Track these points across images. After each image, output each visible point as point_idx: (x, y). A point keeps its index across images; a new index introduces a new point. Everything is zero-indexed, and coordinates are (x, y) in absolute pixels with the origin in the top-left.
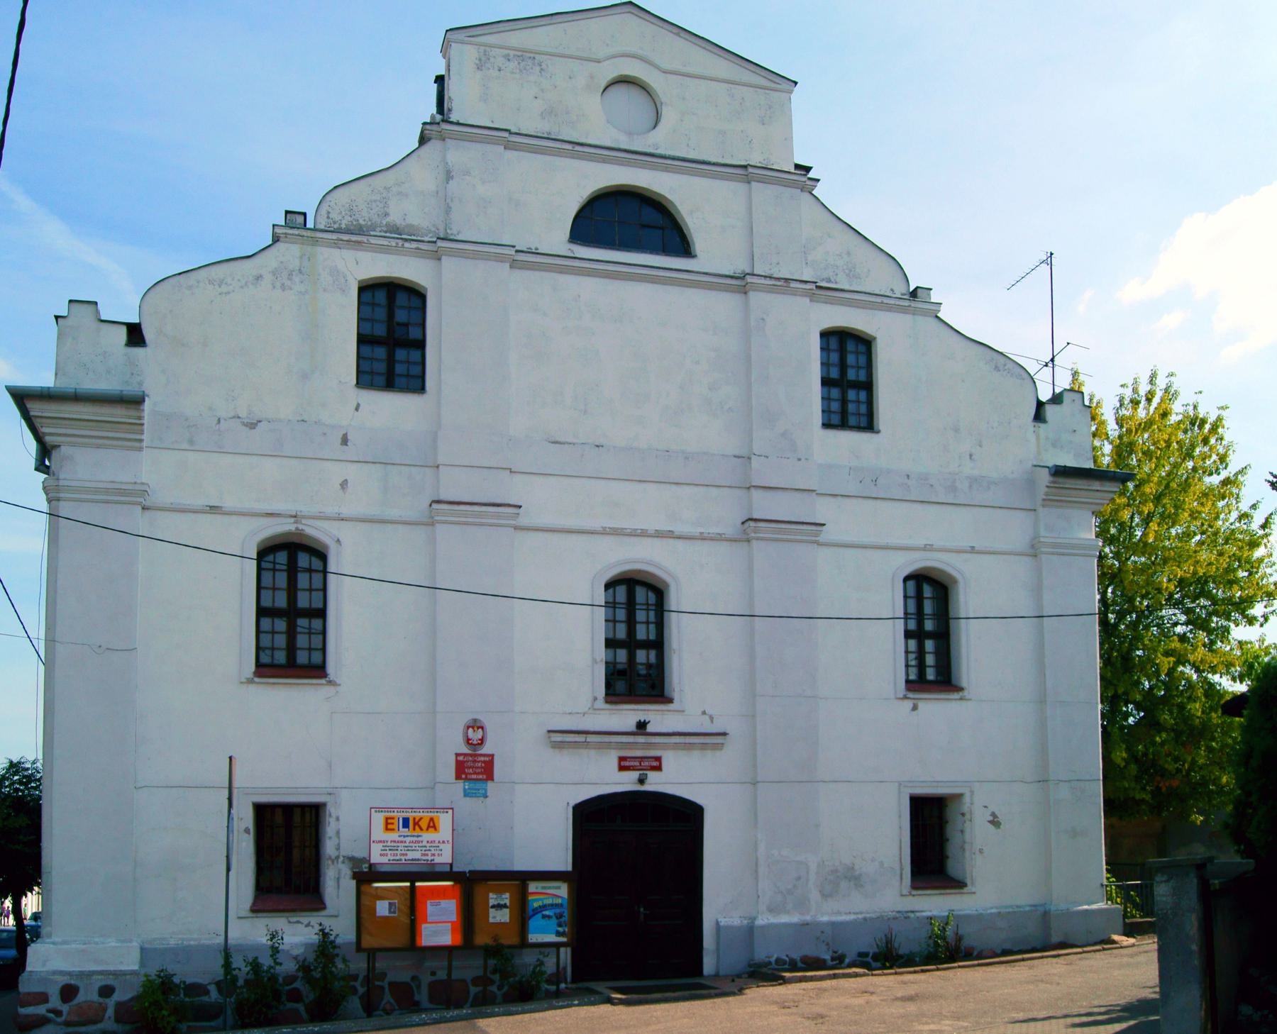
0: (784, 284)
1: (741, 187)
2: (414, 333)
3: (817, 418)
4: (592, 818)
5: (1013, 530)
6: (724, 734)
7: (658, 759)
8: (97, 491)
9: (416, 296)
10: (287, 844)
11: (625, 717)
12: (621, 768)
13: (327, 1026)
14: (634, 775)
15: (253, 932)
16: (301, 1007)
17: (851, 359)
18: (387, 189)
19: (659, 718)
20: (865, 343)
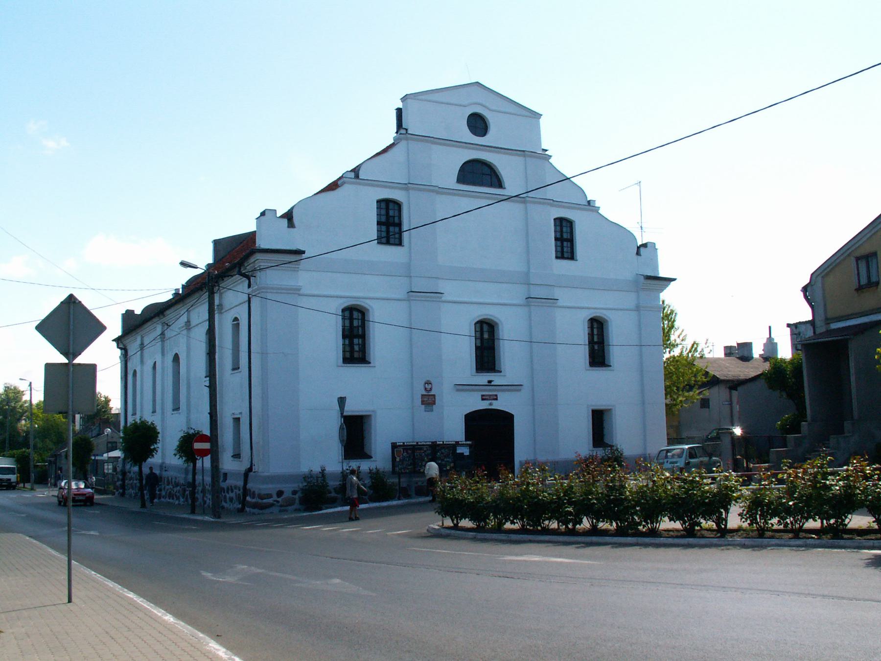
1: (521, 159)
3: (554, 255)
4: (473, 420)
5: (629, 300)
8: (287, 289)
9: (398, 205)
10: (355, 431)
12: (483, 399)
16: (366, 497)
17: (564, 229)
19: (497, 379)
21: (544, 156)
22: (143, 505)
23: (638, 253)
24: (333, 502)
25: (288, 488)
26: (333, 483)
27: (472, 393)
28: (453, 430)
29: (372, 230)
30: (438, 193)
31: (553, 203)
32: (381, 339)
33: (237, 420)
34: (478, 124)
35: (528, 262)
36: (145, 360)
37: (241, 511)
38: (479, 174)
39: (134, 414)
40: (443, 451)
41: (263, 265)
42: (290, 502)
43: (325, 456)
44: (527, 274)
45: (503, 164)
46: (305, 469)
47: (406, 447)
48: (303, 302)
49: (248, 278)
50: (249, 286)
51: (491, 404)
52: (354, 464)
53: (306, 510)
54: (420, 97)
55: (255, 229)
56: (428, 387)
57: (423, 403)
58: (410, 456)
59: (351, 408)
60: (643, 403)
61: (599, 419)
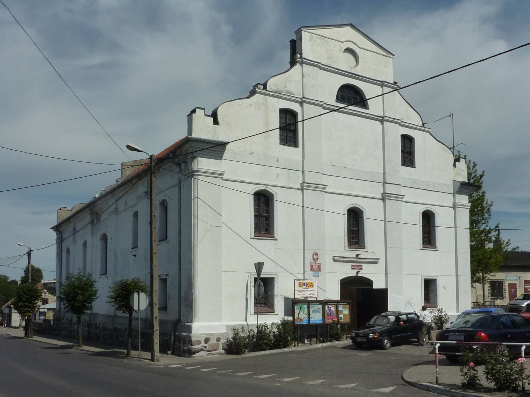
0: (393, 121)
5: (449, 200)
6: (379, 259)
10: (264, 291)
11: (352, 253)
12: (353, 269)
13: (239, 357)
14: (356, 271)
15: (253, 321)
18: (286, 79)
45: (369, 90)
56: (316, 257)
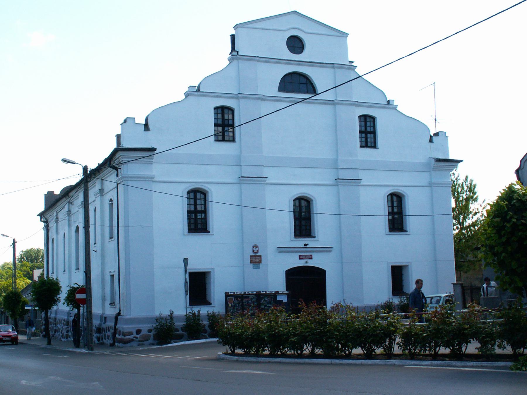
2: (231, 122)
3: (358, 144)
4: (292, 275)
5: (423, 178)
7: (311, 255)
8: (144, 178)
9: (231, 110)
10: (198, 285)
11: (300, 243)
12: (300, 259)
16: (206, 334)
17: (368, 124)
20: (373, 119)
21: (350, 66)
22: (49, 343)
23: (431, 140)
24: (180, 338)
25: (145, 328)
26: (179, 324)
27: (292, 254)
28: (276, 282)
29: (211, 130)
30: (262, 100)
31: (358, 104)
32: (218, 215)
33: (112, 276)
34: (296, 44)
35: (337, 151)
36: (59, 231)
37: (112, 345)
38: (297, 84)
39: (53, 273)
40: (266, 299)
41: (125, 160)
42: (146, 339)
43: (175, 304)
44: (336, 161)
46: (157, 314)
47: (236, 296)
48: (156, 187)
49: (117, 169)
50: (117, 175)
51: (307, 262)
52: (195, 309)
53: (158, 344)
54: (247, 26)
55: (120, 133)
57: (251, 262)
58: (238, 302)
59: (193, 267)
60: (436, 260)
61: (398, 273)
